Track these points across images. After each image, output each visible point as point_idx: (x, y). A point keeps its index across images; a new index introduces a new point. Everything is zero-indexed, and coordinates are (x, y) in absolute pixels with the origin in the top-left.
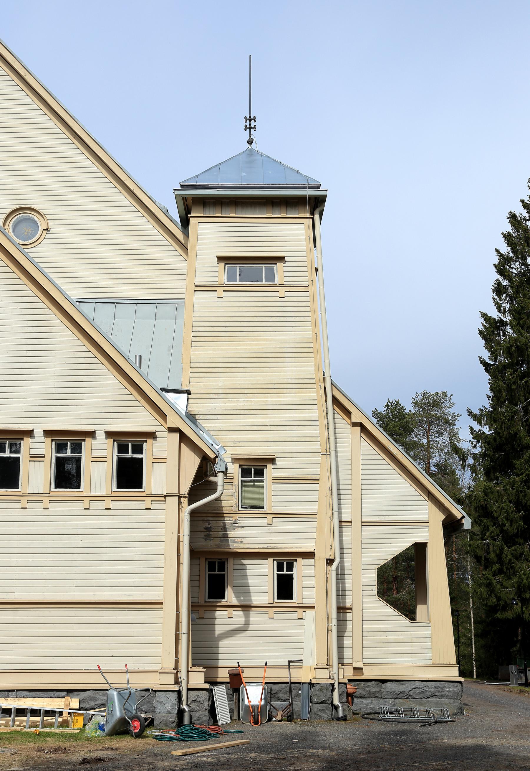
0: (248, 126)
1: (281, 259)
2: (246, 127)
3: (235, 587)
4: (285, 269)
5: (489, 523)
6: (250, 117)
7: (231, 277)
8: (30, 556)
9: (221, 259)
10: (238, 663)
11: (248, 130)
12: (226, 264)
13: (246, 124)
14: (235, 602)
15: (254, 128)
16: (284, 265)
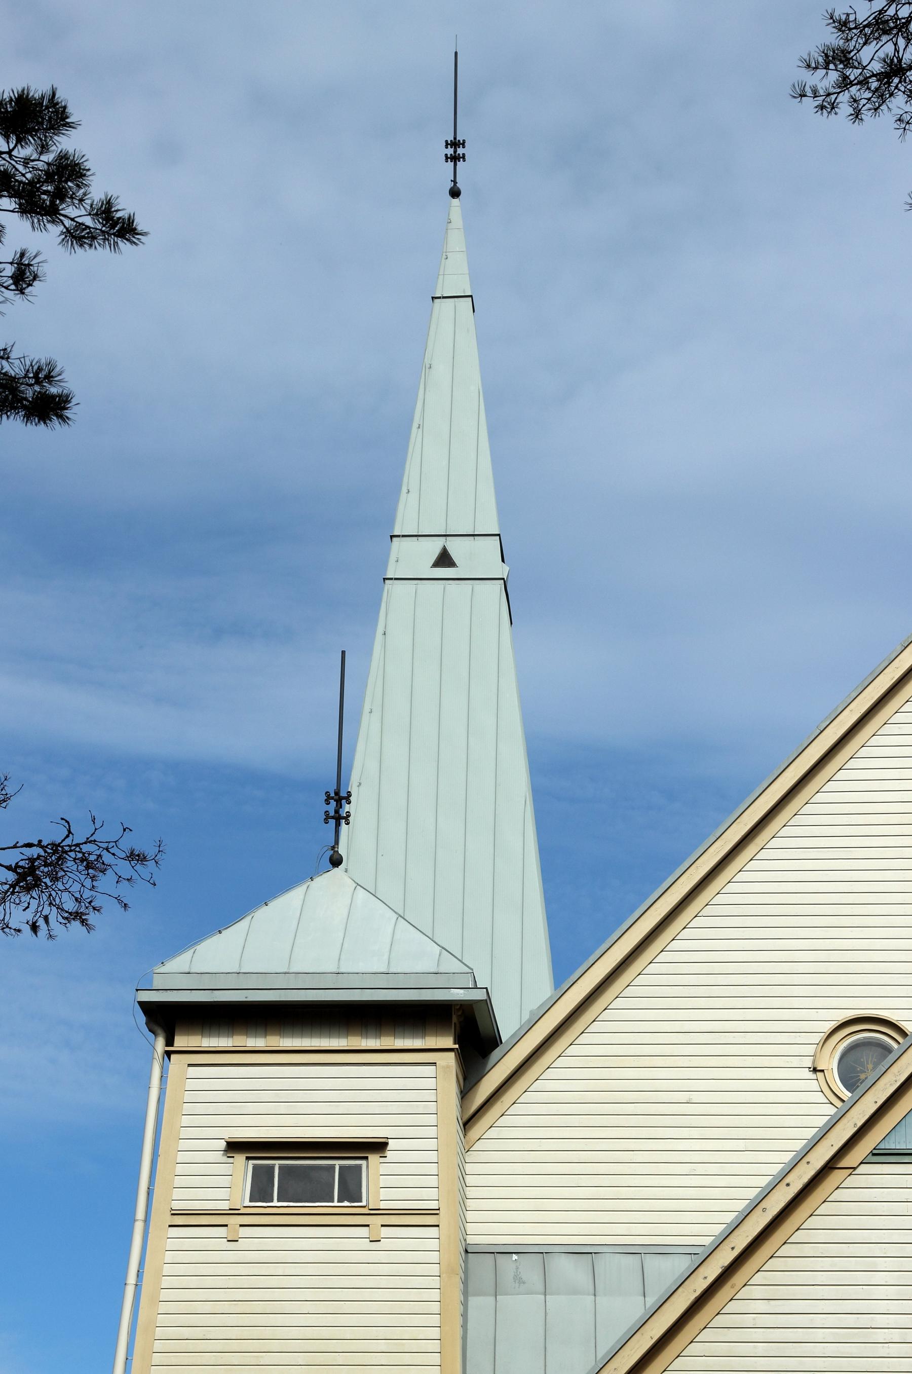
0: (332, 813)
1: (379, 1147)
2: (327, 817)
3: (157, 1341)
4: (384, 1169)
5: (889, 49)
6: (337, 793)
7: (261, 1191)
8: (695, 1097)
9: (234, 1147)
10: (342, 651)
11: (332, 822)
12: (248, 1158)
13: (327, 808)
14: (26, 286)
15: (347, 818)
16: (382, 1160)
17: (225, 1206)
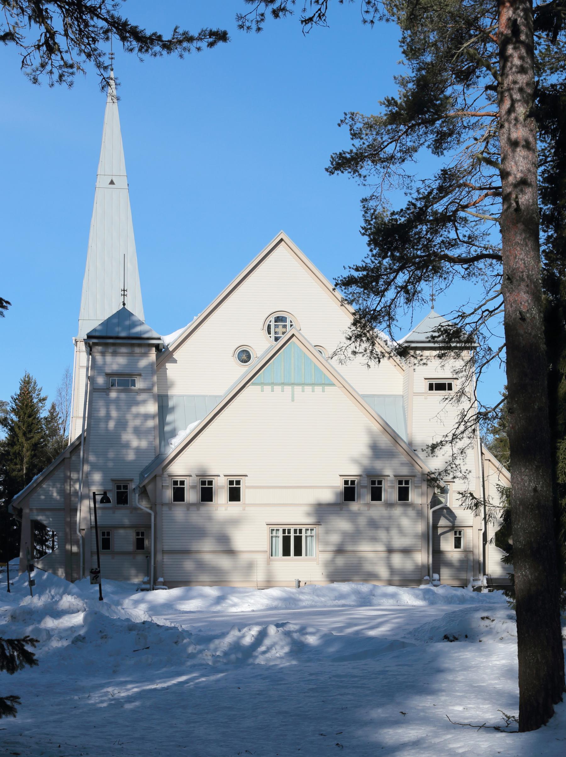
17: (105, 387)
